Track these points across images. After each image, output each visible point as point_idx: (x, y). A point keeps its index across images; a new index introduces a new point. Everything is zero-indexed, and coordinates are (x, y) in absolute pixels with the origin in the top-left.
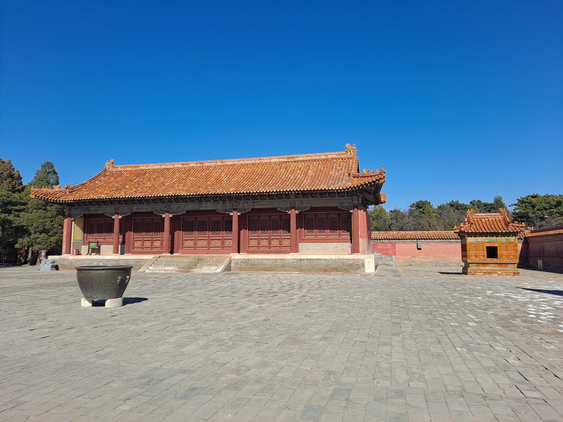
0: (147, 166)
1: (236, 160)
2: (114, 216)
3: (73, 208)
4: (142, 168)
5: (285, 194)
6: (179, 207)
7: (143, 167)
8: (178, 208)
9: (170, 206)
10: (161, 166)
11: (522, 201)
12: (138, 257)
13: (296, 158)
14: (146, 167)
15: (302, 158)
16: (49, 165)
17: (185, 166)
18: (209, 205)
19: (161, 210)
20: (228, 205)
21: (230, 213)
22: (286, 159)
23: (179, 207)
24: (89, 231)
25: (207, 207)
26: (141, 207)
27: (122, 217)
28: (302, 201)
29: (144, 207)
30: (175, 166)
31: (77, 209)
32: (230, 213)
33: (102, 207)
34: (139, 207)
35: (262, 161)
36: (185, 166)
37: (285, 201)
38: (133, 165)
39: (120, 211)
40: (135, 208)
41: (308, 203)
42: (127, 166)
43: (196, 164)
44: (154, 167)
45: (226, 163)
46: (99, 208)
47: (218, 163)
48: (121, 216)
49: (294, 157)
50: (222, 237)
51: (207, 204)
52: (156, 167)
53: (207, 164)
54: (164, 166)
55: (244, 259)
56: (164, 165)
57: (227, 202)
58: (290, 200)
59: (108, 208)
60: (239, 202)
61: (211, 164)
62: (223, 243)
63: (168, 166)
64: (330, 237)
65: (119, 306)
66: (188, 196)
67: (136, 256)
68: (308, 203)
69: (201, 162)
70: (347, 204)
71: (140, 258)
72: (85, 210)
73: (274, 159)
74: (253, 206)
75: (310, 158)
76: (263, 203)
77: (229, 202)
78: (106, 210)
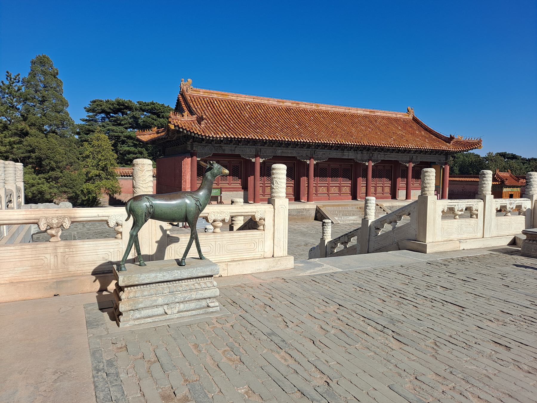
0: (237, 96)
1: (329, 106)
2: (254, 159)
3: (201, 145)
4: (231, 97)
5: (425, 151)
6: (324, 154)
7: (232, 96)
8: (323, 155)
9: (315, 152)
10: (254, 100)
11: (54, 104)
12: (301, 207)
13: (376, 113)
14: (236, 98)
15: (380, 114)
16: (42, 61)
17: (281, 104)
18: (351, 154)
19: (306, 156)
20: (366, 155)
21: (366, 163)
22: (368, 112)
23: (324, 154)
24: (239, 175)
25: (348, 156)
26: (286, 151)
27: (317, 162)
28: (417, 156)
29: (289, 151)
30: (270, 102)
31: (205, 146)
32: (366, 163)
33: (240, 148)
34: (284, 151)
35: (350, 111)
36: (281, 104)
37: (406, 155)
38: (219, 92)
39: (262, 154)
40: (279, 151)
41: (421, 158)
42: (212, 91)
43: (292, 103)
44: (246, 99)
45: (320, 107)
46: (236, 147)
47: (313, 106)
48: (262, 159)
49: (375, 112)
50: (217, 184)
51: (349, 153)
52: (249, 99)
53: (303, 105)
54: (258, 100)
55: (389, 206)
56: (258, 99)
57: (365, 152)
58: (409, 154)
59: (247, 149)
60: (374, 154)
61: (307, 106)
62: (340, 190)
63: (262, 101)
64: (233, 185)
65: (369, 250)
66: (350, 146)
67: (298, 206)
68: (421, 158)
69: (297, 102)
70: (443, 161)
71: (302, 208)
72: (217, 149)
73: (360, 110)
74: (384, 157)
75: (385, 114)
76: (391, 156)
77: (366, 152)
78: (246, 152)
